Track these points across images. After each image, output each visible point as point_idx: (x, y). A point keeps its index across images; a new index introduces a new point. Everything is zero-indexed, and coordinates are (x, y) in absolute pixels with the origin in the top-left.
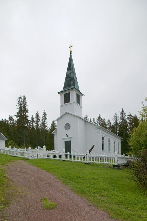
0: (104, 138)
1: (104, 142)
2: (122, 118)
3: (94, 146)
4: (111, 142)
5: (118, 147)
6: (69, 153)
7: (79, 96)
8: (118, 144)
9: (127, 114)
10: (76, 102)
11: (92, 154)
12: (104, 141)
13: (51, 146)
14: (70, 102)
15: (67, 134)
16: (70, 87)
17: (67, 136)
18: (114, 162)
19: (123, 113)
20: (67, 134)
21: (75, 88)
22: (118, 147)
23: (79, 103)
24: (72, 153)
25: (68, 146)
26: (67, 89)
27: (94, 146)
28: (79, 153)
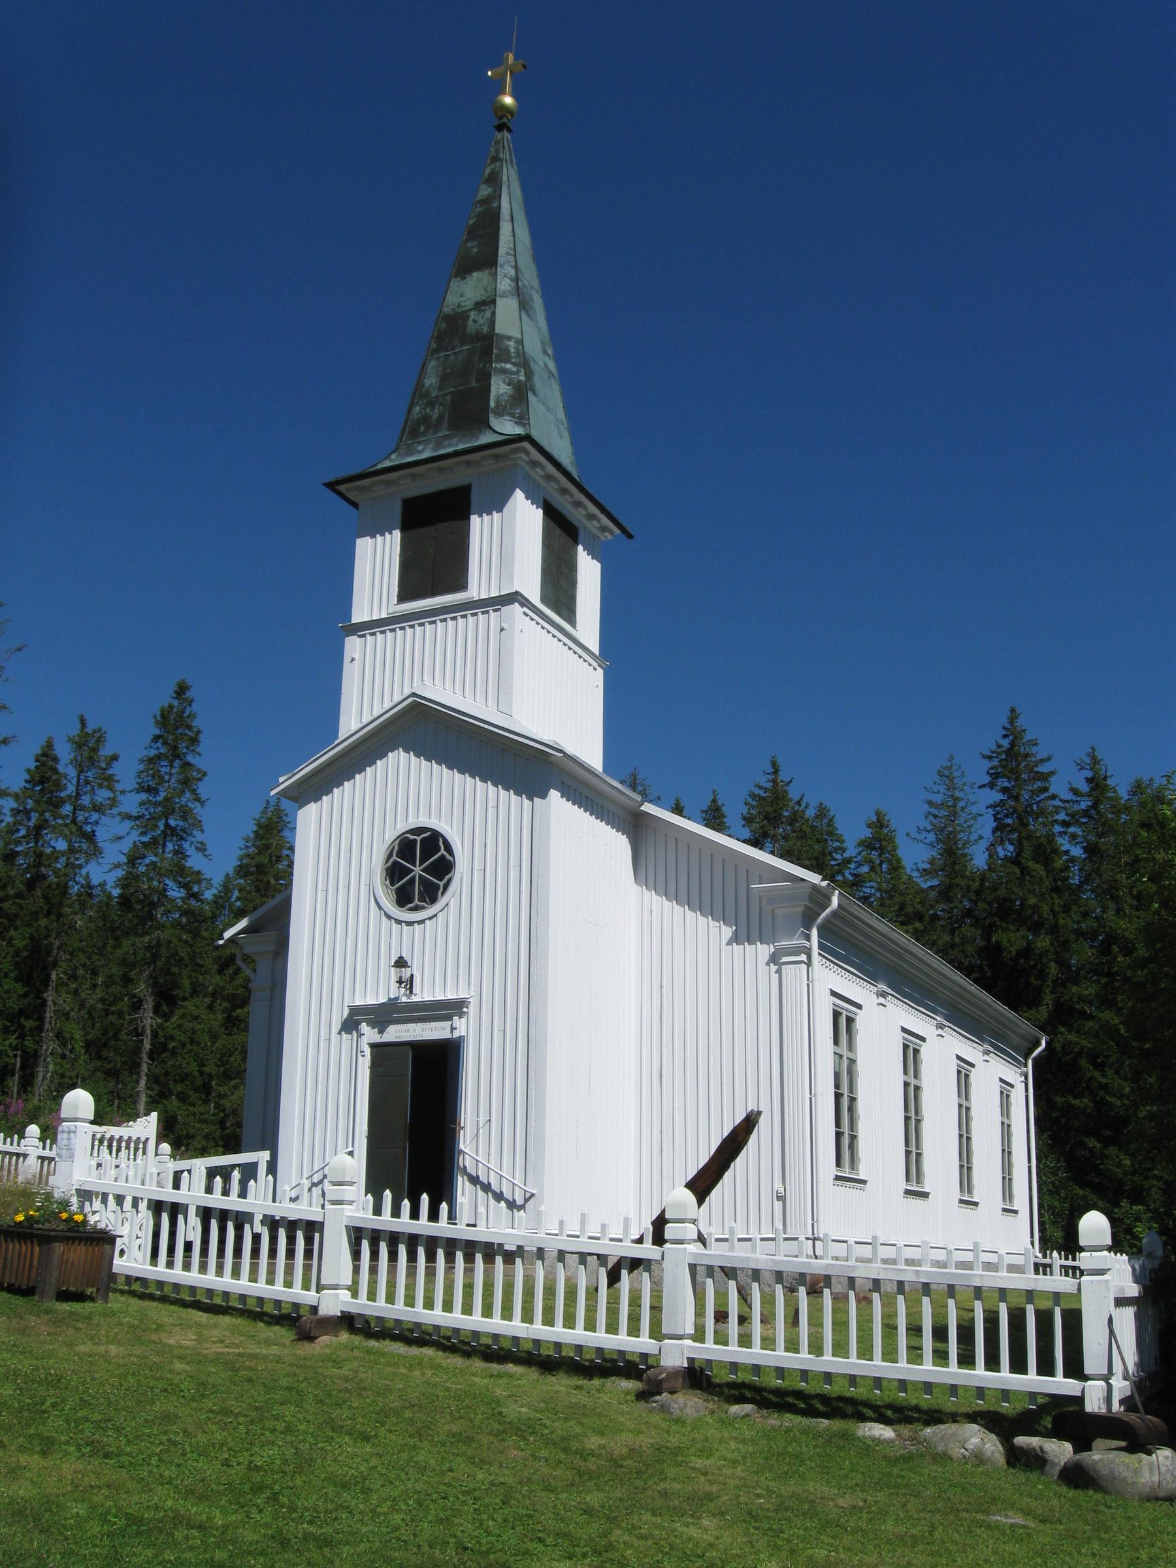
0: (850, 1021)
1: (851, 1072)
2: (1015, 819)
3: (748, 1124)
4: (924, 1069)
5: (1006, 1129)
6: (415, 1215)
7: (543, 600)
8: (1005, 1098)
9: (1066, 781)
10: (533, 592)
11: (737, 1223)
12: (917, 1089)
13: (215, 1096)
14: (462, 586)
15: (401, 963)
16: (475, 436)
17: (408, 984)
18: (1075, 1369)
19: (1013, 763)
20: (401, 963)
21: (528, 438)
22: (1006, 1129)
23: (572, 599)
24: (472, 1215)
25: (419, 1113)
26: (439, 446)
27: (748, 1124)
28: (156, 804)
